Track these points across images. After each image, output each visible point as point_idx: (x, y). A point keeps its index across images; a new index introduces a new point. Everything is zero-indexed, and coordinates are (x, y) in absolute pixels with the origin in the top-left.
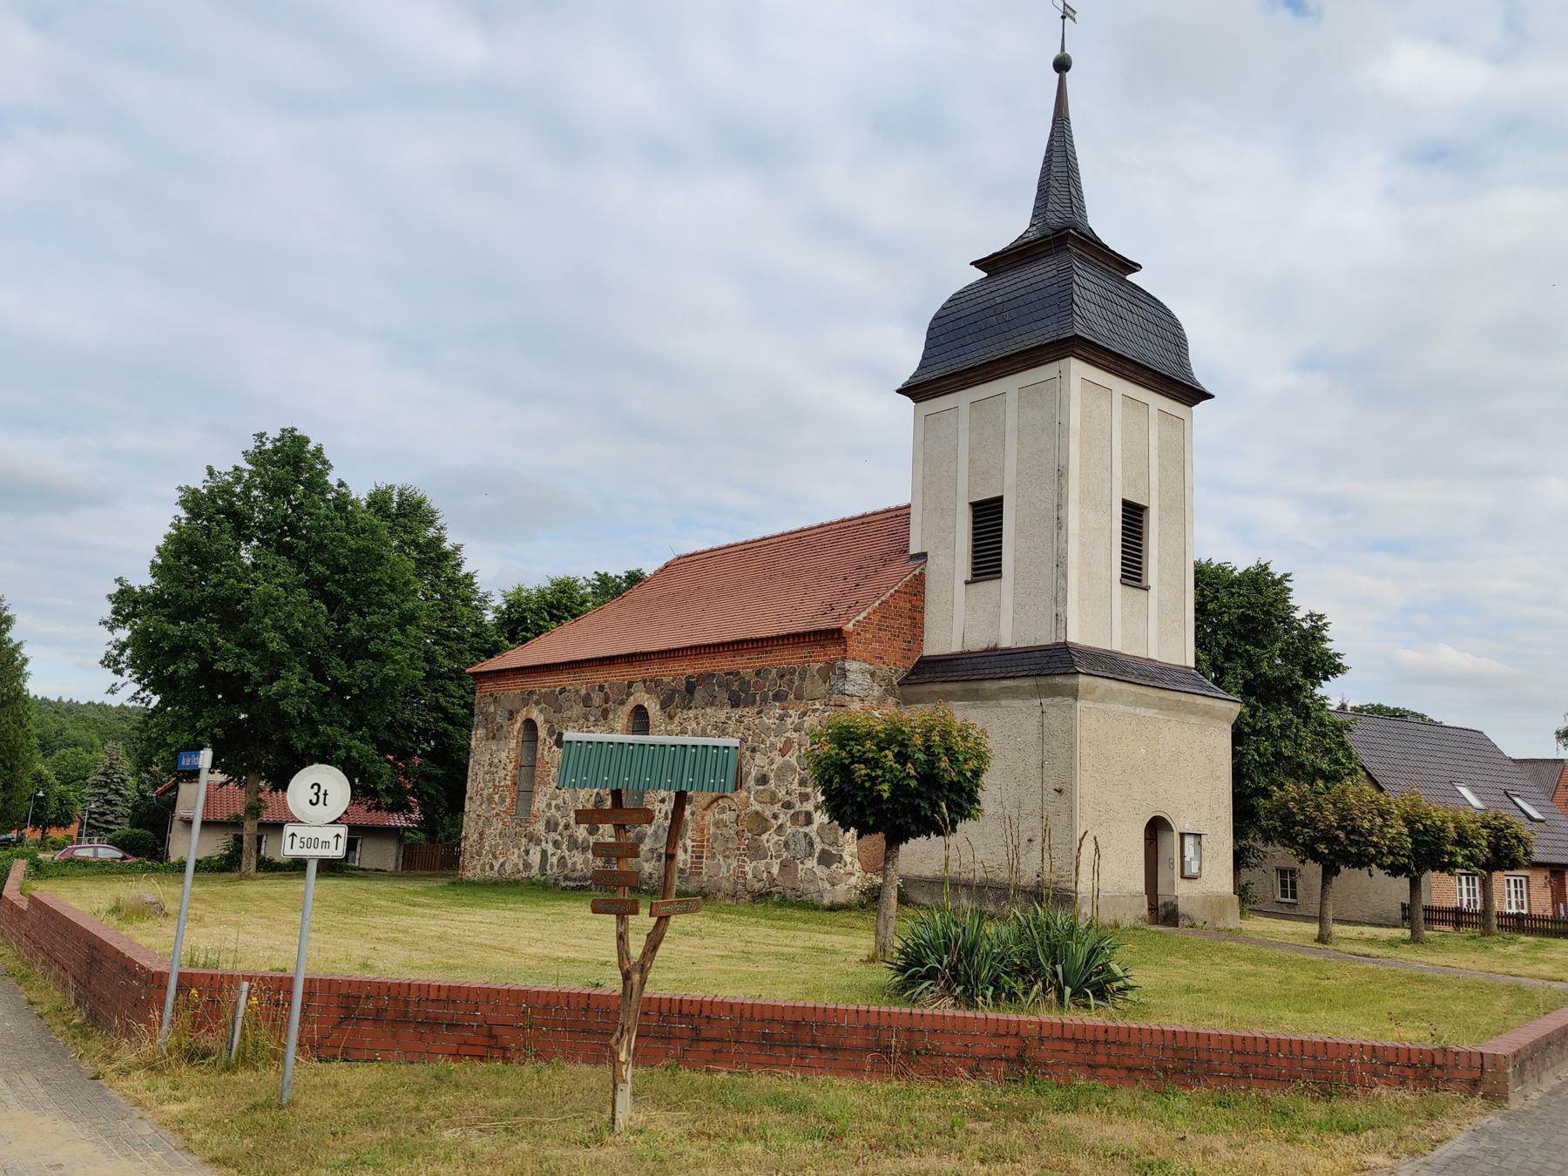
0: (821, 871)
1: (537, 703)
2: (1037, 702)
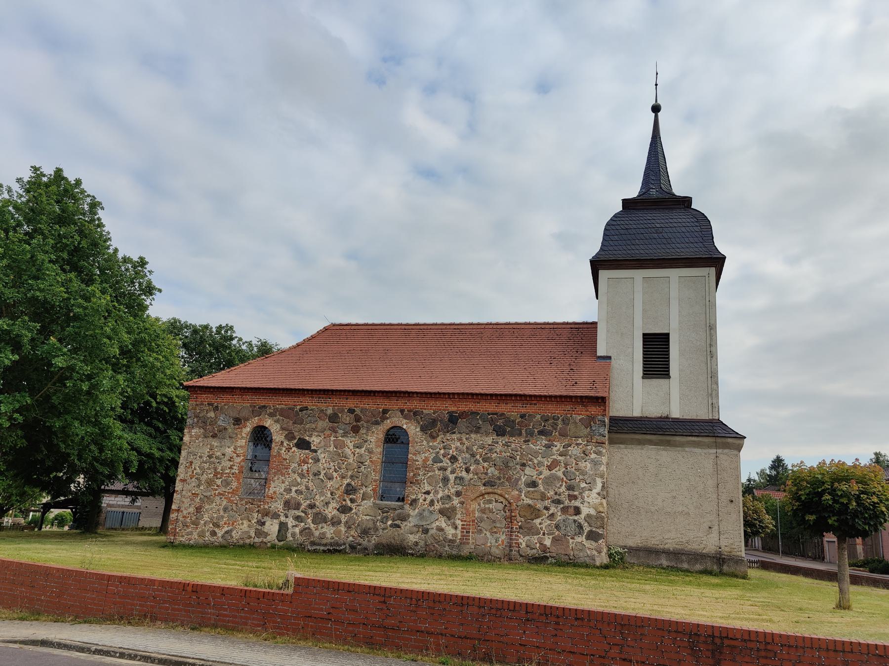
0: (588, 544)
1: (271, 415)
2: (714, 451)
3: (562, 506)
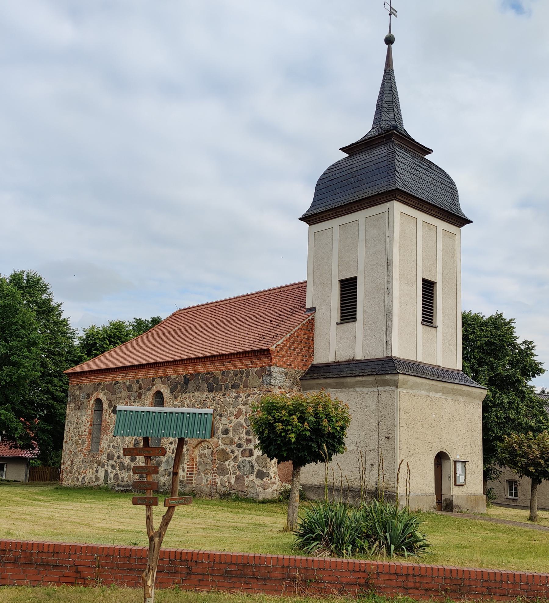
0: (258, 482)
1: (103, 390)
2: (376, 389)
3: (242, 449)
